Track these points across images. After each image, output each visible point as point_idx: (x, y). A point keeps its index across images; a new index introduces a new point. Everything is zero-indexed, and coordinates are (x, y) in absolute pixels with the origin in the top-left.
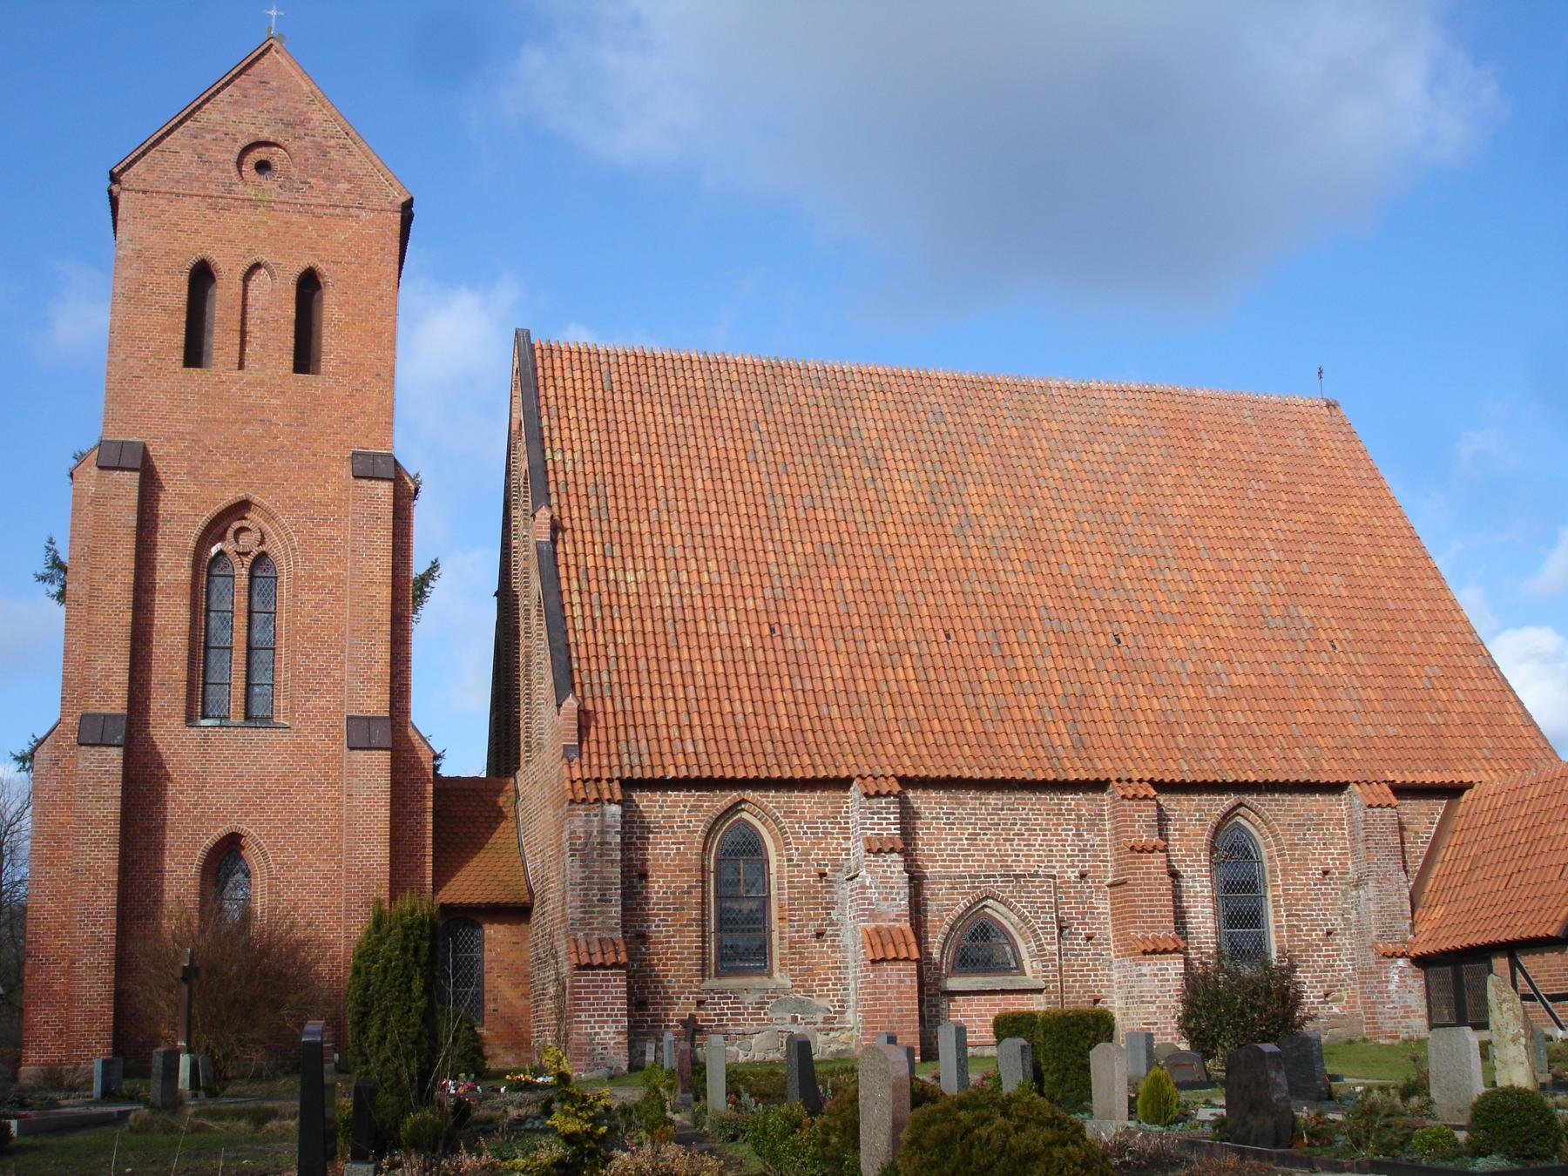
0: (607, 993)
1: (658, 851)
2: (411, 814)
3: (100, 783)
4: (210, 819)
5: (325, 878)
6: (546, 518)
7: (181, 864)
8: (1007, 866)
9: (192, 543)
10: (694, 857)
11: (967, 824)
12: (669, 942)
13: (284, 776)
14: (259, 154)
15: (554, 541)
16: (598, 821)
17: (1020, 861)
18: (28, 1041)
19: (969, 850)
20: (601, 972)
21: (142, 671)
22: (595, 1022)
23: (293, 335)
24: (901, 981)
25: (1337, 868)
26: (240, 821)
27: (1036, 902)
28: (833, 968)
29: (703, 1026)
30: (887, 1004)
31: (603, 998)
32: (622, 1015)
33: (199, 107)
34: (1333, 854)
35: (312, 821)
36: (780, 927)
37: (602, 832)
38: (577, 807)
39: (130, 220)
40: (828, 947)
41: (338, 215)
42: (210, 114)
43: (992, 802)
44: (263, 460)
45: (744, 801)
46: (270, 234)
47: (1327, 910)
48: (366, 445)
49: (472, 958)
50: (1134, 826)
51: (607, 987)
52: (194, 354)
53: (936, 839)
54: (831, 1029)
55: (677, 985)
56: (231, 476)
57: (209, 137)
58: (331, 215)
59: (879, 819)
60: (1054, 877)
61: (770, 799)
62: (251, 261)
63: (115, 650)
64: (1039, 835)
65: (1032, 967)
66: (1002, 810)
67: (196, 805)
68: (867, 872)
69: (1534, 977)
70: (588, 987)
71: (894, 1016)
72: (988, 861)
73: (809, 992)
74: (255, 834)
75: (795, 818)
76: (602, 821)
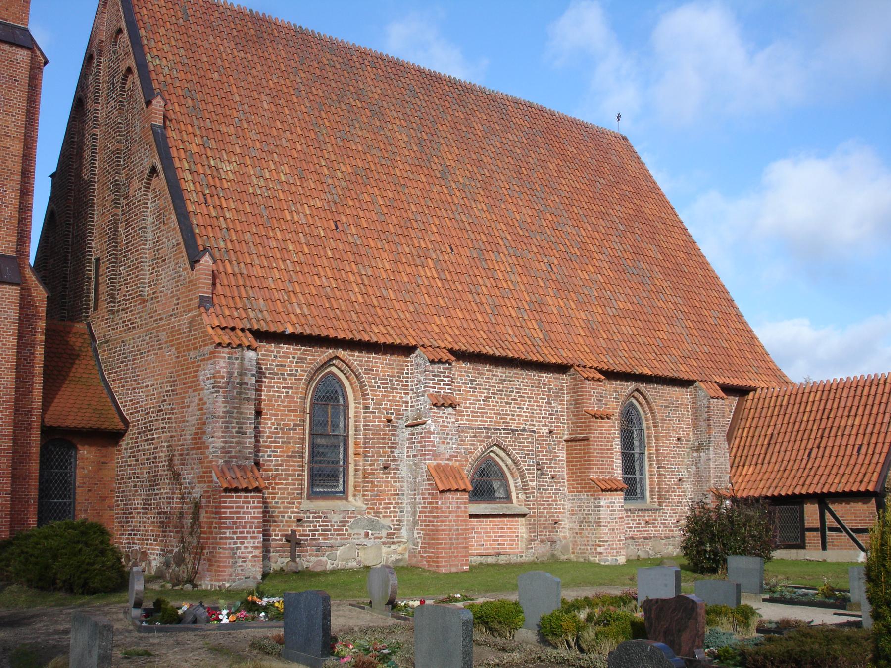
0: (248, 513)
1: (272, 393)
8: (507, 423)
10: (299, 400)
11: (483, 389)
15: (165, 127)
16: (238, 364)
17: (515, 420)
19: (484, 409)
20: (243, 494)
22: (238, 538)
24: (458, 507)
25: (684, 437)
27: (524, 450)
28: (394, 495)
29: (301, 540)
30: (449, 525)
32: (259, 532)
34: (683, 427)
36: (355, 461)
37: (241, 374)
38: (222, 350)
40: (392, 478)
43: (500, 374)
45: (337, 357)
47: (679, 464)
49: (66, 475)
50: (590, 400)
51: (248, 508)
53: (464, 399)
54: (393, 543)
59: (438, 380)
60: (534, 432)
61: (355, 358)
64: (526, 401)
65: (518, 497)
66: (505, 380)
68: (432, 421)
69: (841, 517)
70: (232, 507)
71: (453, 535)
72: (496, 418)
73: (377, 513)
75: (372, 374)
76: (242, 364)
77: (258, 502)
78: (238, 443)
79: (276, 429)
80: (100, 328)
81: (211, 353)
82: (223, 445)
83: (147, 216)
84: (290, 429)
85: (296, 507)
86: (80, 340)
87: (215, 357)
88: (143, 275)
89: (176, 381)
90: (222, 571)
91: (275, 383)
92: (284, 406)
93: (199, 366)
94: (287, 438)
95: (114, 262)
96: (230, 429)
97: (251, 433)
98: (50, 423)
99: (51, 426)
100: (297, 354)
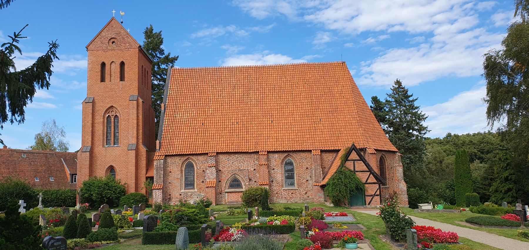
9: (103, 115)
13: (120, 155)
14: (112, 40)
33: (101, 33)
42: (103, 34)
52: (103, 80)
57: (103, 38)
61: (194, 158)
62: (112, 61)
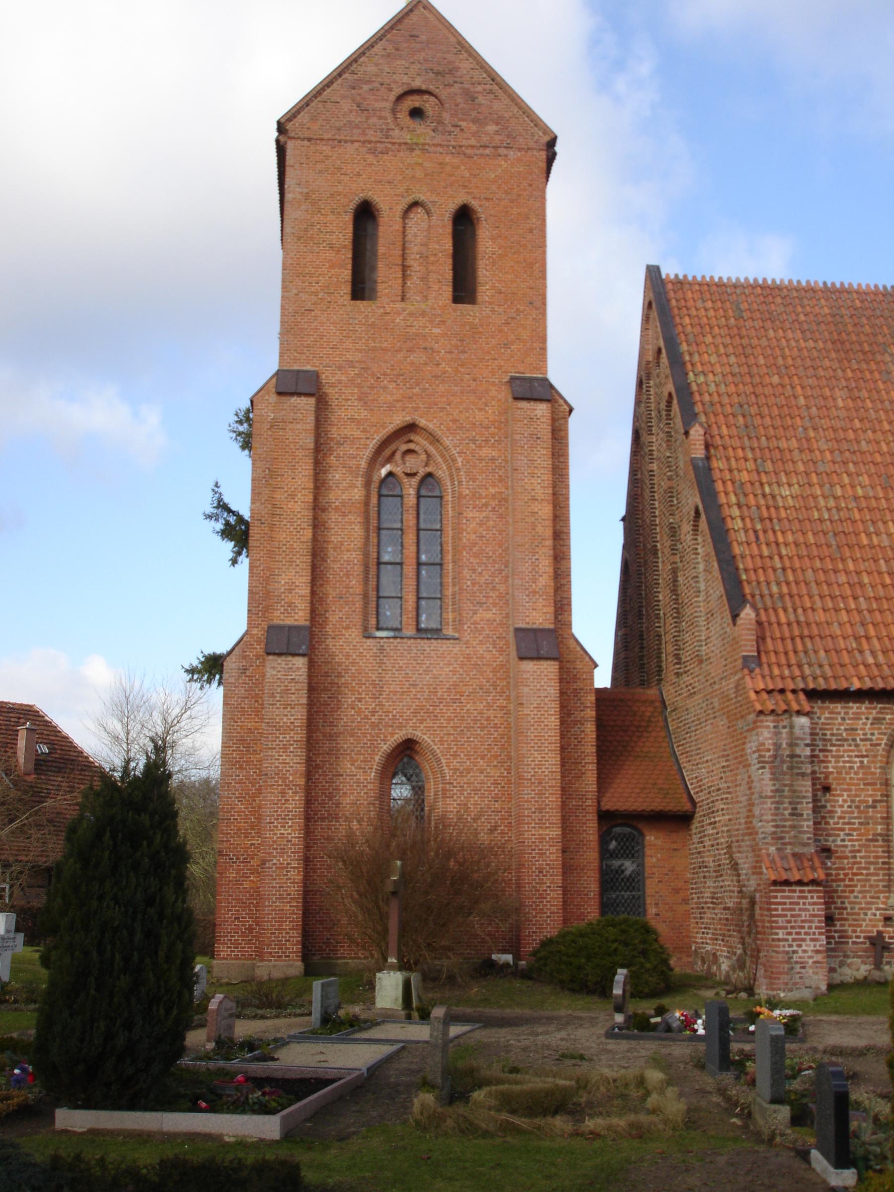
0: (805, 910)
1: (841, 764)
2: (576, 722)
3: (286, 691)
4: (387, 726)
5: (496, 783)
6: (700, 435)
7: (361, 768)
9: (363, 464)
10: (878, 771)
12: (855, 857)
13: (455, 685)
15: (708, 458)
16: (787, 733)
18: (221, 936)
20: (798, 888)
21: (321, 585)
22: (794, 940)
23: (451, 267)
26: (415, 728)
31: (800, 916)
32: (820, 934)
35: (482, 728)
37: (791, 745)
39: (297, 166)
41: (488, 155)
44: (427, 385)
46: (426, 175)
48: (522, 370)
55: (863, 901)
56: (398, 401)
57: (366, 87)
58: (482, 155)
62: (409, 199)
63: (297, 565)
67: (373, 712)
70: (785, 903)
74: (429, 741)
76: (791, 733)
77: (818, 897)
78: (793, 827)
79: (849, 807)
80: (669, 692)
81: (755, 722)
82: (773, 829)
83: (698, 563)
84: (868, 807)
85: (883, 903)
86: (650, 709)
87: (757, 727)
88: (698, 631)
89: (728, 755)
90: (775, 978)
91: (845, 751)
92: (858, 779)
93: (745, 737)
94: (866, 818)
95: (675, 617)
96: (781, 811)
97: (808, 815)
98: (607, 807)
99: (608, 811)
100: (871, 713)
